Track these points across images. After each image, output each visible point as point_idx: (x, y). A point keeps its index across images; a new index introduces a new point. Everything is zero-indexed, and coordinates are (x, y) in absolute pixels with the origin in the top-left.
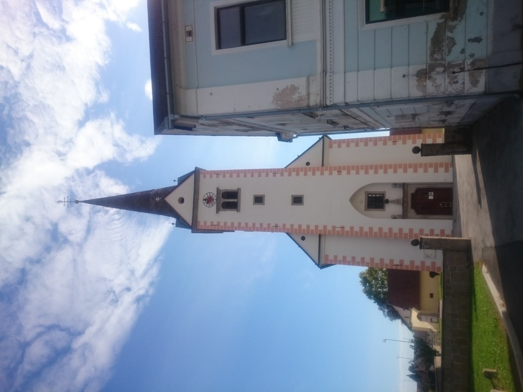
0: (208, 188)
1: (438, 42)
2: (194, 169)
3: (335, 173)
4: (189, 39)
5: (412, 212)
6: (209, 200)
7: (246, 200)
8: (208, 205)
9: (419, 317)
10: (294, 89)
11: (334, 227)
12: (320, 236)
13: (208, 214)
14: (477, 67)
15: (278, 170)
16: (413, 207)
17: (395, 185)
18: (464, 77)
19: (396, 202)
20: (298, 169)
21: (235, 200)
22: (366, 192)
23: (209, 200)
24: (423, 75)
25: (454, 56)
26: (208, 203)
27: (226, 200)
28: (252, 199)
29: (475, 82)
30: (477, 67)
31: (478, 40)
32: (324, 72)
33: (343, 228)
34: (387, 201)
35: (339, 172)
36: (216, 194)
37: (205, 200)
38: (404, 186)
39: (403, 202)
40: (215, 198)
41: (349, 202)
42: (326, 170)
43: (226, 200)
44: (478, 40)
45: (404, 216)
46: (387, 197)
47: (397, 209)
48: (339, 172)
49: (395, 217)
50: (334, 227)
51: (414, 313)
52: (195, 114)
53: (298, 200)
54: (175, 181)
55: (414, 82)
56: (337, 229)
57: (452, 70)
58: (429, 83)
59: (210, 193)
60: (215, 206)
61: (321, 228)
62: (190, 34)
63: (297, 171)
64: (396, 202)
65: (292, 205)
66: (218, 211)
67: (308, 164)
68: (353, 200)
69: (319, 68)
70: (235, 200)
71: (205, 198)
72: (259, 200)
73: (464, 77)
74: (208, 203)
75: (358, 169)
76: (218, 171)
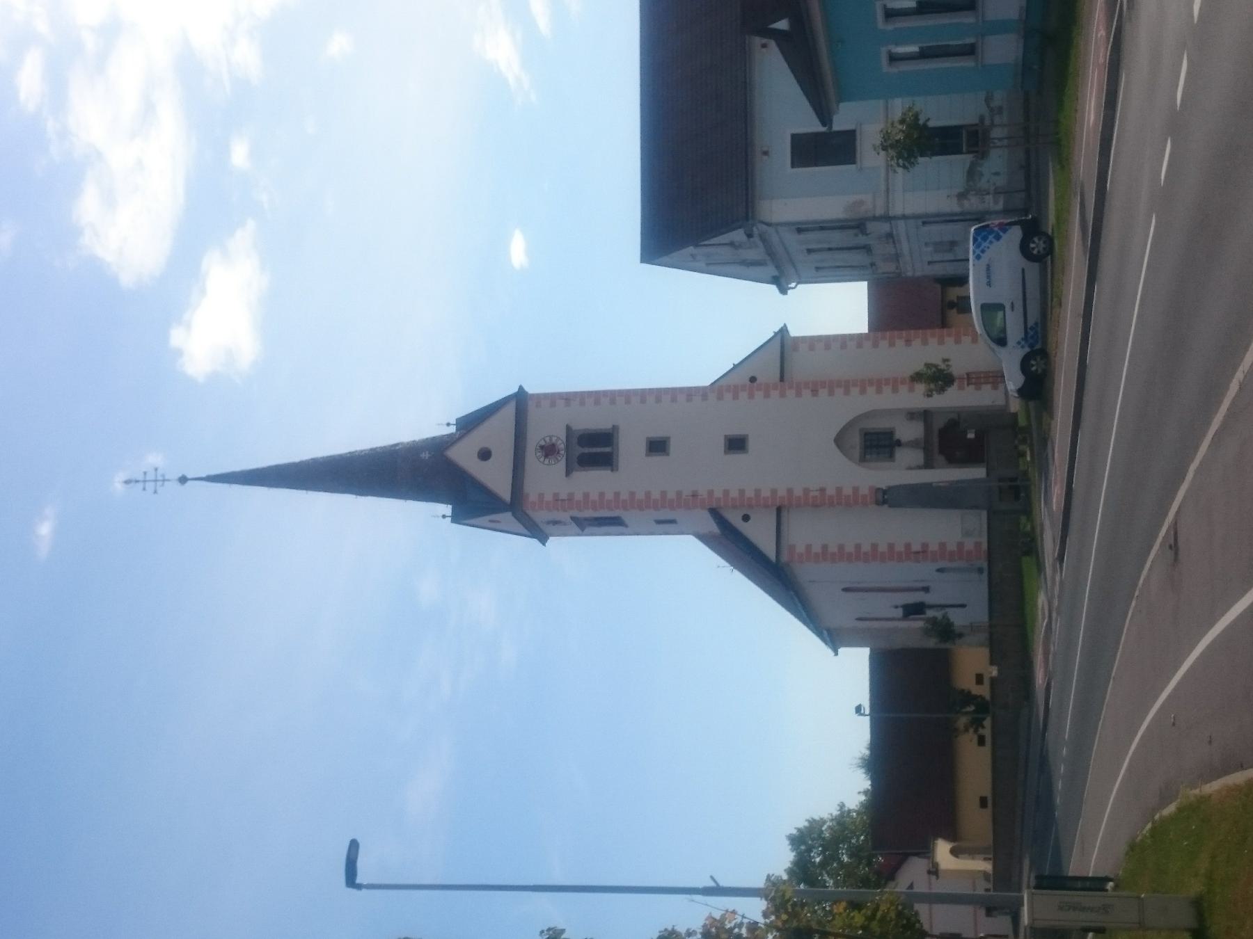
0: (543, 429)
1: (972, 173)
2: (516, 390)
3: (807, 393)
4: (765, 158)
5: (941, 459)
6: (549, 451)
7: (630, 448)
8: (547, 461)
9: (954, 852)
10: (861, 203)
11: (806, 491)
12: (779, 510)
13: (546, 478)
14: (997, 192)
15: (697, 389)
16: (941, 452)
17: (912, 415)
18: (989, 198)
19: (914, 444)
20: (736, 387)
21: (607, 450)
22: (861, 430)
23: (549, 451)
24: (962, 196)
25: (983, 183)
26: (546, 456)
27: (586, 450)
28: (642, 447)
29: (996, 202)
30: (997, 192)
31: (997, 174)
32: (888, 190)
33: (822, 490)
34: (899, 443)
35: (815, 392)
36: (564, 439)
37: (542, 447)
38: (926, 416)
39: (925, 445)
40: (562, 446)
41: (834, 445)
42: (791, 388)
43: (586, 450)
44: (997, 174)
45: (928, 464)
46: (898, 436)
47: (918, 456)
48: (815, 392)
49: (910, 468)
50: (806, 491)
51: (942, 849)
52: (768, 220)
53: (736, 444)
54: (448, 424)
55: (955, 200)
56: (812, 494)
57: (981, 193)
58: (966, 203)
59: (551, 437)
60: (563, 462)
61: (782, 492)
62: (766, 153)
63: (735, 391)
64: (914, 444)
65: (726, 453)
66: (568, 472)
67: (753, 379)
68: (840, 441)
69: (883, 187)
70: (607, 450)
71: (543, 443)
72: (657, 446)
73: (989, 198)
74: (546, 456)
75: (847, 386)
76: (567, 393)
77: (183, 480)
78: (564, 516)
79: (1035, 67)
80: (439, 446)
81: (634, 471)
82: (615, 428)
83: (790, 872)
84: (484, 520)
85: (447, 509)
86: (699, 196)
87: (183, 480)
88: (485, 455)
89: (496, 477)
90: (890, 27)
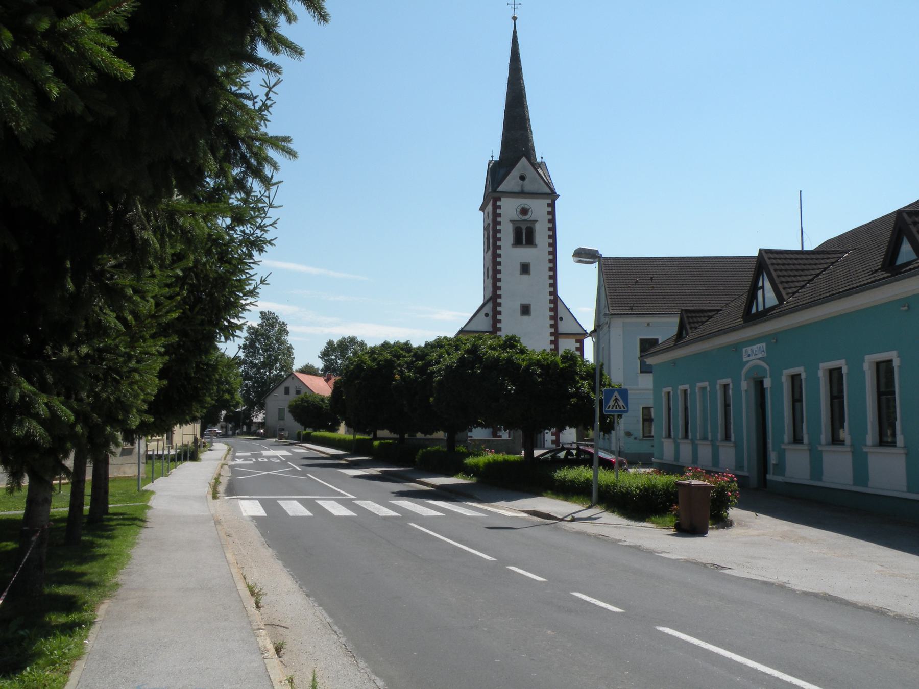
0: (538, 208)
6: (524, 211)
7: (525, 254)
13: (509, 208)
21: (524, 242)
60: (516, 218)
70: (524, 242)
77: (515, 19)
78: (490, 220)
79: (278, 365)
80: (529, 152)
81: (512, 256)
82: (535, 246)
83: (371, 348)
84: (489, 179)
85: (497, 158)
86: (629, 283)
87: (515, 19)
88: (522, 178)
89: (510, 183)
90: (718, 387)
